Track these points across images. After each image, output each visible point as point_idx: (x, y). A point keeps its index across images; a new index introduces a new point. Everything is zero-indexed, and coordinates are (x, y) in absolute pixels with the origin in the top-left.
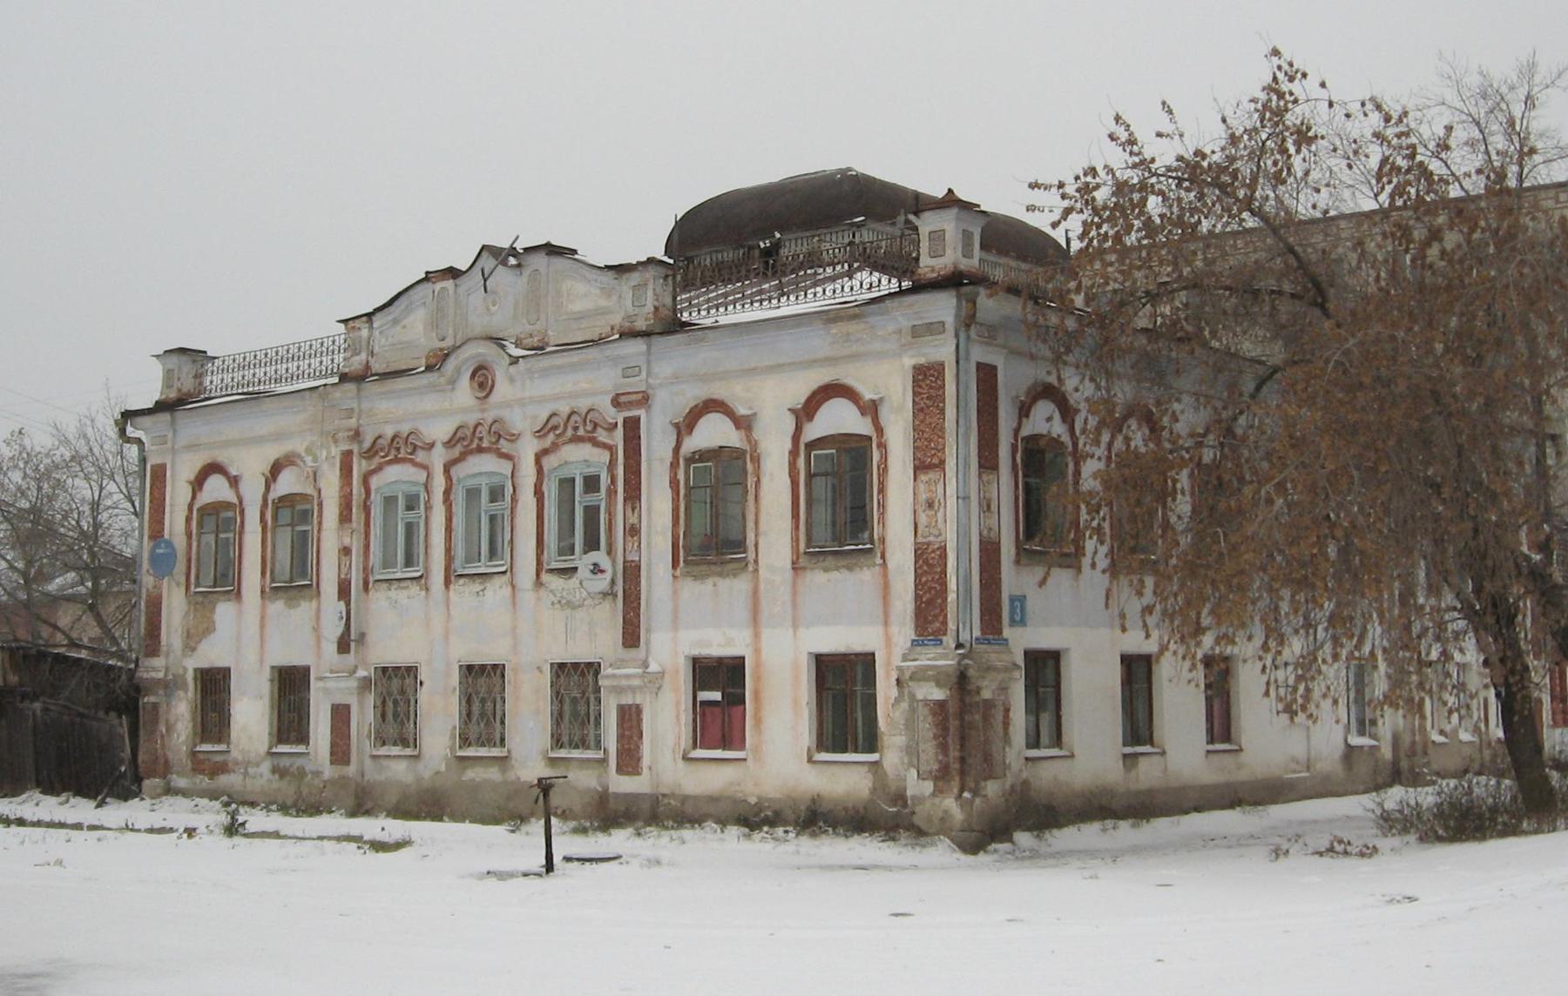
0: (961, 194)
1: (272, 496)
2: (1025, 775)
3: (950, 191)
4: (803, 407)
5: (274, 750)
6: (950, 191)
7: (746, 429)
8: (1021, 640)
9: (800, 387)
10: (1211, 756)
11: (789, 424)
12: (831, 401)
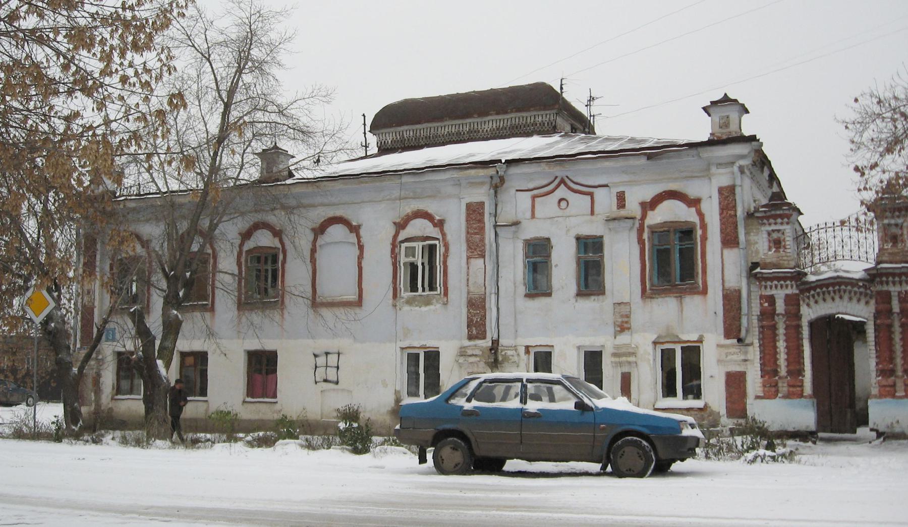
0: (732, 96)
1: (246, 248)
2: (110, 406)
3: (726, 94)
4: (319, 227)
5: (116, 397)
6: (726, 94)
7: (439, 226)
8: (183, 345)
9: (242, 224)
10: (245, 404)
11: (392, 230)
12: (334, 226)
